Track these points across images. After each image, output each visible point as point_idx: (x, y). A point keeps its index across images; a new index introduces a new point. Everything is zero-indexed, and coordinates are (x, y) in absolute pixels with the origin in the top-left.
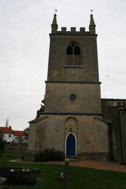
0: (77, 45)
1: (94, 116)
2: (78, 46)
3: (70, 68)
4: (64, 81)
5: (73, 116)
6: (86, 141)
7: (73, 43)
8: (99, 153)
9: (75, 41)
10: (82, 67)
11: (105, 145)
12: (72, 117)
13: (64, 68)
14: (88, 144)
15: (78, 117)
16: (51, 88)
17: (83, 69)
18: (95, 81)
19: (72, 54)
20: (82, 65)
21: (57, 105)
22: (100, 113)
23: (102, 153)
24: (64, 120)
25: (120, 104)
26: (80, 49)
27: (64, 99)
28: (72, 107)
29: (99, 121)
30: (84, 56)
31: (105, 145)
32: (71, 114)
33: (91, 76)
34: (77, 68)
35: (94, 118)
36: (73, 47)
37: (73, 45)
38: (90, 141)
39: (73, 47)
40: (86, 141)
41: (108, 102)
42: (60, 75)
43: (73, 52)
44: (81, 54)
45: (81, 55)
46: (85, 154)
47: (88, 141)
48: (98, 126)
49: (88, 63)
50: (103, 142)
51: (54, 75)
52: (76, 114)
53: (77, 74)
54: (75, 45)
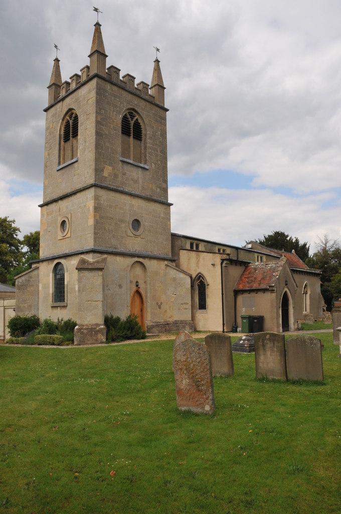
0: (137, 120)
1: (166, 262)
2: (140, 121)
3: (130, 165)
4: (122, 189)
5: (141, 260)
6: (157, 303)
7: (132, 113)
8: (175, 321)
9: (136, 109)
10: (147, 169)
11: (186, 309)
12: (139, 262)
13: (120, 163)
14: (160, 307)
15: (146, 262)
16: (104, 201)
17: (147, 172)
18: (162, 199)
19: (130, 136)
20: (145, 163)
21: (114, 236)
22: (170, 256)
23: (181, 321)
24: (128, 266)
25: (179, 243)
26: (141, 128)
27: (123, 225)
28: (135, 244)
29: (175, 271)
30: (149, 146)
31: (186, 309)
32: (139, 256)
33: (158, 190)
34: (140, 169)
35: (166, 265)
36: (132, 120)
37: (132, 117)
38: (161, 303)
39: (132, 120)
40: (157, 303)
41: (206, 249)
42: (116, 176)
43: (132, 130)
44: (143, 139)
45: (143, 142)
46: (158, 325)
47: (159, 304)
48: (174, 279)
49: (155, 164)
50: (182, 304)
51: (106, 174)
52: (144, 257)
53: (140, 181)
54: (135, 118)
